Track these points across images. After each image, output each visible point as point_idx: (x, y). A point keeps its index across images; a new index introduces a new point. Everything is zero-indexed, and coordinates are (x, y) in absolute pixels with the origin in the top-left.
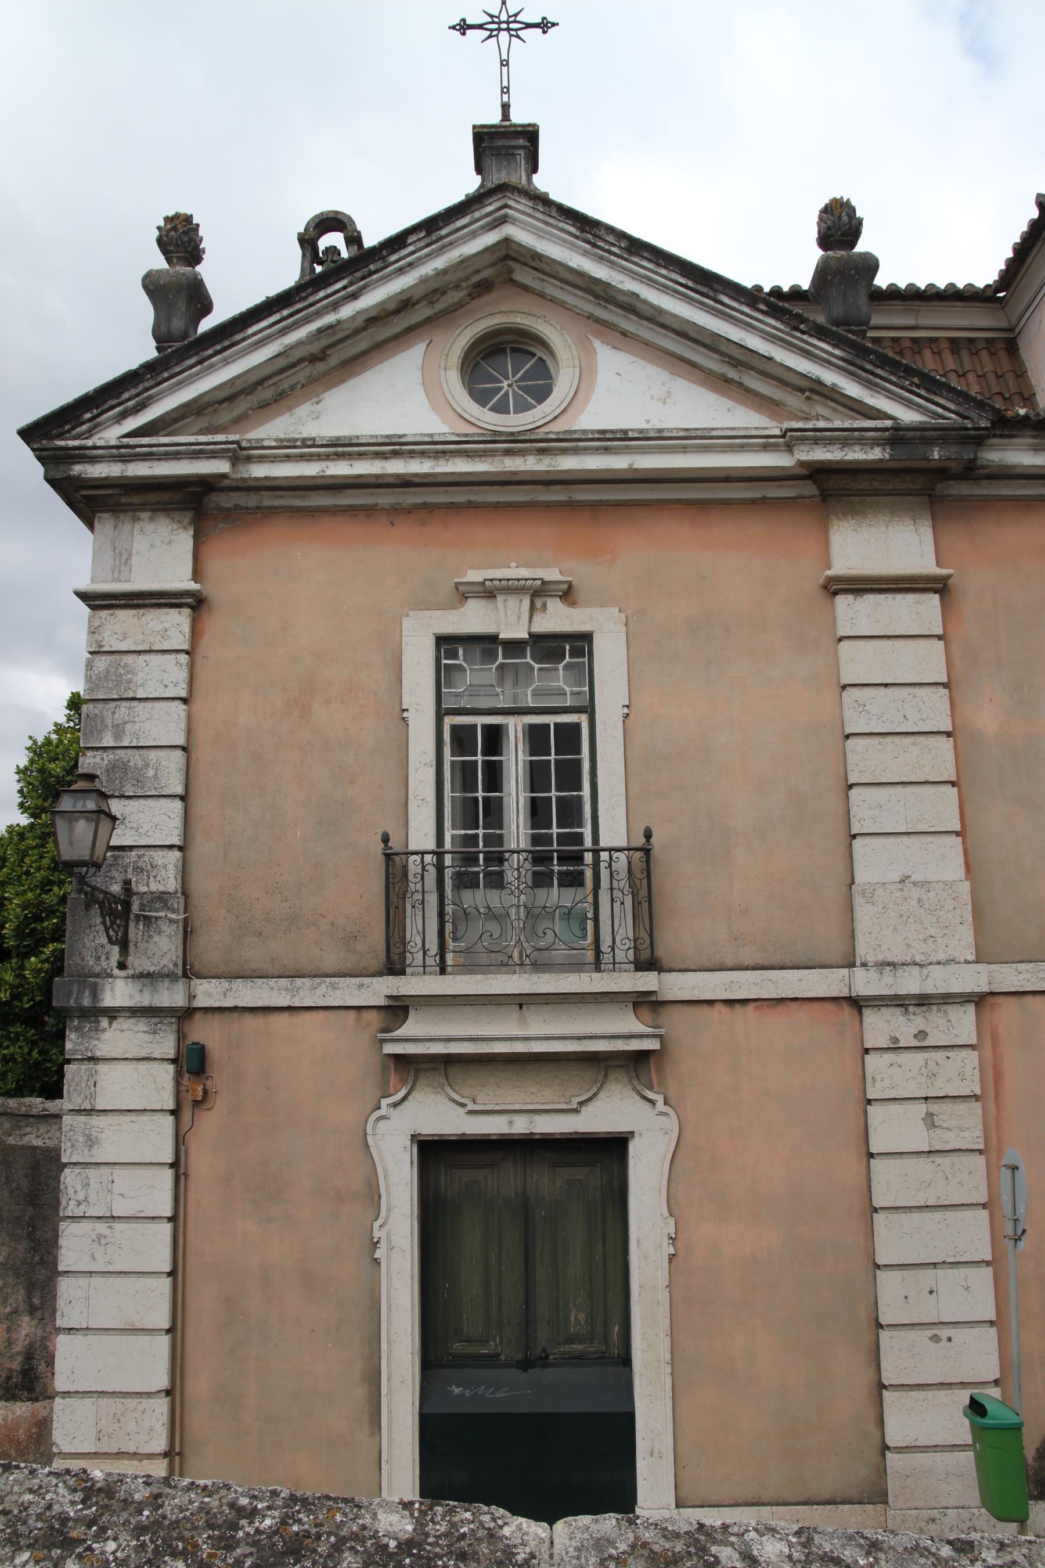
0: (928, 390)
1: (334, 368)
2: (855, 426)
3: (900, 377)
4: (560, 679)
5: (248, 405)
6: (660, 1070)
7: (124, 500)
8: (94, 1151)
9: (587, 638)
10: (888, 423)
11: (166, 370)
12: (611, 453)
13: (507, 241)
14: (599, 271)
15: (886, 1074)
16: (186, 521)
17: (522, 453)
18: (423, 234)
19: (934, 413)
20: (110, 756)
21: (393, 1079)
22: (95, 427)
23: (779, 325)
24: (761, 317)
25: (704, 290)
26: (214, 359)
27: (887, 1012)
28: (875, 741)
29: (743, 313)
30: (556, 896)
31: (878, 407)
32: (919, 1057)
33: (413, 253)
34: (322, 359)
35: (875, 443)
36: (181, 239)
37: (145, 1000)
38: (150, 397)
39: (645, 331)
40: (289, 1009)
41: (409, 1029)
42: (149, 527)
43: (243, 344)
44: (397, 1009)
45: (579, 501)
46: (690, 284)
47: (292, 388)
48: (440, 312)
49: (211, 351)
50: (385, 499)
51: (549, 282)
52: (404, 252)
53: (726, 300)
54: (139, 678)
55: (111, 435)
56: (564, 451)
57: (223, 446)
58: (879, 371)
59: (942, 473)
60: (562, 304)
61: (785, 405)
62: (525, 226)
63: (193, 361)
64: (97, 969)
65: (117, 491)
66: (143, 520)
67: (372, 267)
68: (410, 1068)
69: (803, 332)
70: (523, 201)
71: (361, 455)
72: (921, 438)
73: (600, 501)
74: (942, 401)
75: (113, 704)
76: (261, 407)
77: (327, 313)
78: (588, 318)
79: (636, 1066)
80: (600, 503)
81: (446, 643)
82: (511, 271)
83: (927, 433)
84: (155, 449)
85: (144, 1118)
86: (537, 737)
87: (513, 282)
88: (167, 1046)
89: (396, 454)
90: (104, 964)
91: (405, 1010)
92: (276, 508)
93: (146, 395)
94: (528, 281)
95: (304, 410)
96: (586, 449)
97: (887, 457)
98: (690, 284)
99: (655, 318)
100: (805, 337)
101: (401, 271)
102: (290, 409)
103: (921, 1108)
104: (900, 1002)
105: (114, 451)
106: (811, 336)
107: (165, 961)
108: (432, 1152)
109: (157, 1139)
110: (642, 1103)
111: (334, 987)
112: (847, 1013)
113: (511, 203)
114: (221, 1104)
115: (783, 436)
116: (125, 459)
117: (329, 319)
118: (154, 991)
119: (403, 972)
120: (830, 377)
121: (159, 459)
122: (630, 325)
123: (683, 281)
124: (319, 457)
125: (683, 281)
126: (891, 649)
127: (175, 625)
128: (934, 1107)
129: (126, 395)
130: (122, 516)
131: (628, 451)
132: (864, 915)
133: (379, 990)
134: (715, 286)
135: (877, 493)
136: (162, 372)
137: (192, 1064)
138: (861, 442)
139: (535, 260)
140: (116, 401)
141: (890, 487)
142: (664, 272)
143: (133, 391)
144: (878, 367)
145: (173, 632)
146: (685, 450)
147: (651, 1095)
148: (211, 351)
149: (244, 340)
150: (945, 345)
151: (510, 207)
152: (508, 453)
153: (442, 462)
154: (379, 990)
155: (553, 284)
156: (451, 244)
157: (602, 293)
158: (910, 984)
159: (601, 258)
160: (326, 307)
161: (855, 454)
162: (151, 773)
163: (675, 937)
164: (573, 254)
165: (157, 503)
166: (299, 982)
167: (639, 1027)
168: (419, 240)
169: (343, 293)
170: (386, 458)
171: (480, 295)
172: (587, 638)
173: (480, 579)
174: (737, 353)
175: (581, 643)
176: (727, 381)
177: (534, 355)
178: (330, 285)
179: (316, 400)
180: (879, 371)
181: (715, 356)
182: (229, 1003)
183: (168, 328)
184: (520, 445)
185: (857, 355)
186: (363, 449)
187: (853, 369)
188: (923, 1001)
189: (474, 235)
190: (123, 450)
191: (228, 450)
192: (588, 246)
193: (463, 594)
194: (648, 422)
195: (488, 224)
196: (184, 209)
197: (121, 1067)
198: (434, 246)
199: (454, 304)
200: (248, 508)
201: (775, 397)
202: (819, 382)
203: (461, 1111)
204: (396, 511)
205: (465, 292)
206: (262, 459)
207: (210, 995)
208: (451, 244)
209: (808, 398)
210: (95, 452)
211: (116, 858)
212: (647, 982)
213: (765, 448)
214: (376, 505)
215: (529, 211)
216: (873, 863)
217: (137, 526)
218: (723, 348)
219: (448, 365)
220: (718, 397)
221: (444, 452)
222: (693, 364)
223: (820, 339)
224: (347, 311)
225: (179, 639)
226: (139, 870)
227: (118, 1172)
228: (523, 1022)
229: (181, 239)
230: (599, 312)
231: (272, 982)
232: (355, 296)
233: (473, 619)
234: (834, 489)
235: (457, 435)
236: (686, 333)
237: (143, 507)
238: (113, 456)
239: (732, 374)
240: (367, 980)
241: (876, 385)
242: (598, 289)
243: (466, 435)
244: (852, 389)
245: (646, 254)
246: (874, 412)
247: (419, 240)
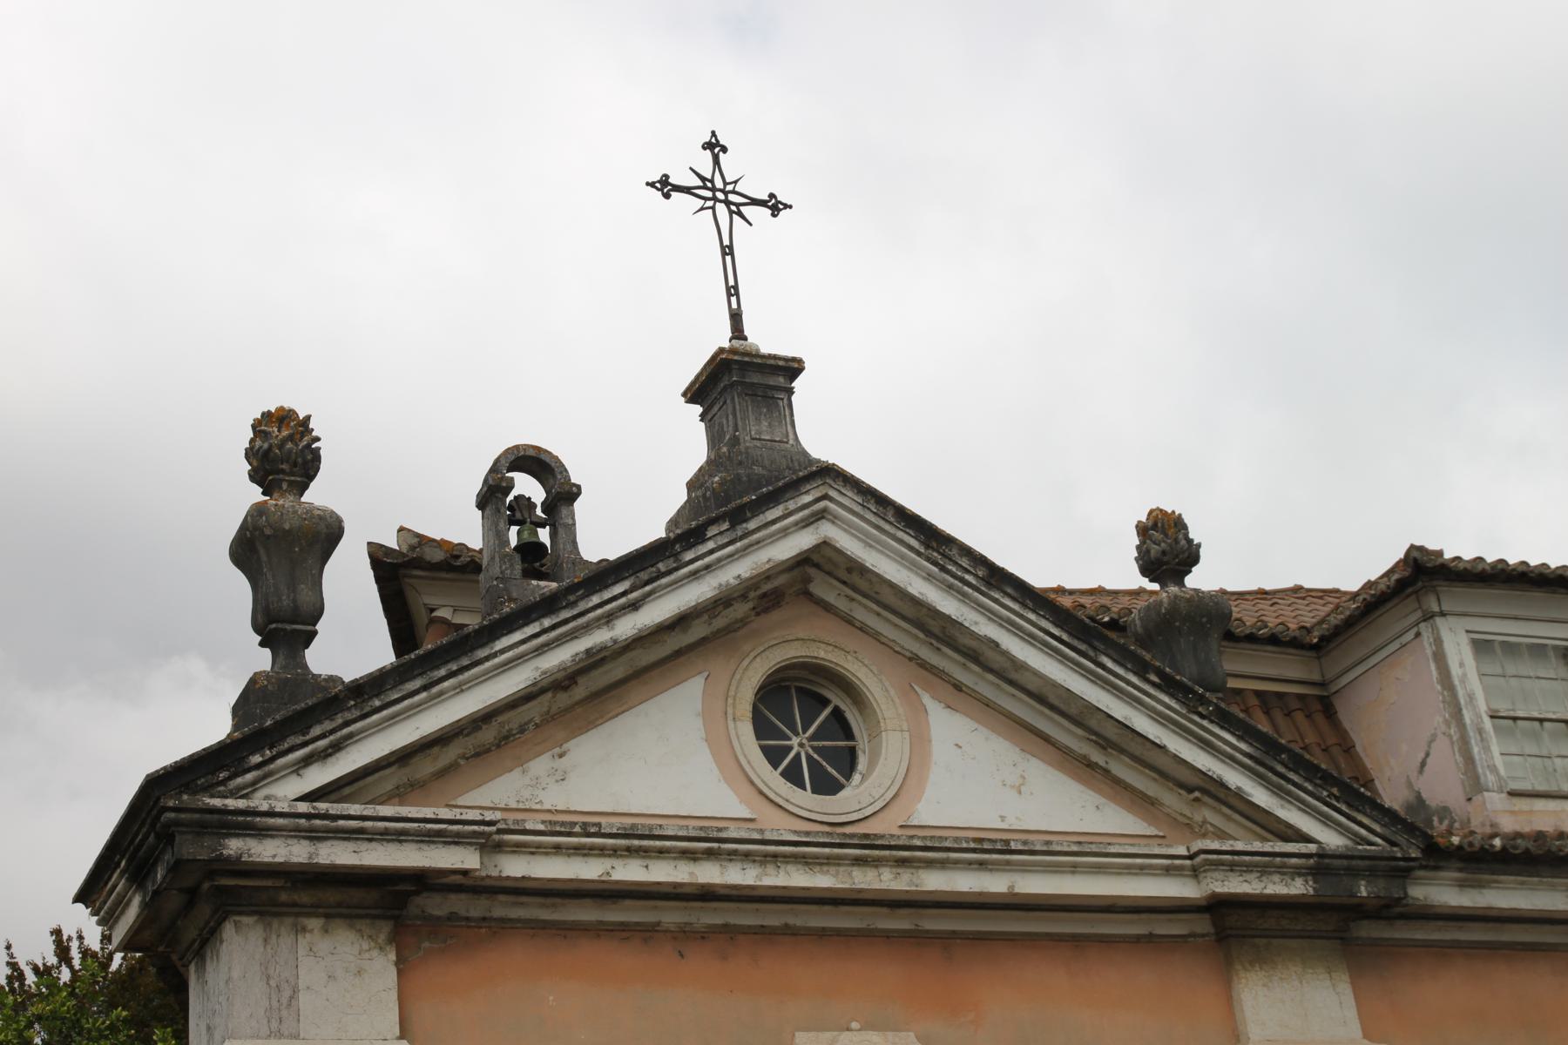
0: (1349, 805)
1: (578, 703)
2: (1277, 849)
3: (1316, 785)
5: (461, 751)
7: (284, 897)
10: (1312, 848)
11: (377, 696)
12: (987, 870)
13: (825, 544)
14: (948, 605)
16: (382, 938)
17: (876, 863)
18: (726, 526)
19: (1356, 834)
22: (265, 777)
23: (1173, 703)
24: (1152, 691)
25: (1083, 647)
26: (446, 684)
29: (1128, 683)
31: (1292, 822)
33: (711, 552)
34: (566, 688)
35: (1298, 872)
38: (351, 736)
39: (986, 686)
42: (324, 945)
43: (488, 665)
45: (928, 931)
46: (1065, 637)
47: (522, 730)
48: (719, 631)
49: (443, 672)
50: (671, 916)
51: (860, 603)
52: (702, 549)
53: (1110, 664)
56: (930, 864)
57: (476, 828)
58: (1292, 776)
59: (1360, 911)
60: (875, 636)
61: (1162, 804)
62: (849, 528)
63: (417, 683)
65: (280, 883)
66: (311, 931)
67: (662, 566)
69: (1202, 717)
70: (849, 494)
72: (1348, 869)
73: (954, 932)
74: (1366, 821)
76: (477, 755)
77: (599, 627)
78: (910, 659)
80: (954, 935)
82: (808, 580)
83: (1354, 863)
84: (368, 824)
87: (808, 595)
89: (710, 854)
92: (511, 920)
93: (346, 731)
94: (831, 598)
95: (541, 765)
96: (957, 862)
97: (1311, 892)
98: (1065, 637)
99: (1009, 673)
100: (1205, 723)
101: (695, 575)
102: (521, 762)
105: (303, 821)
106: (1212, 722)
113: (833, 493)
115: (1190, 857)
116: (314, 836)
117: (600, 637)
120: (1234, 778)
121: (370, 840)
122: (968, 676)
123: (1056, 631)
124: (602, 852)
125: (1056, 631)
129: (316, 731)
130: (275, 923)
131: (1007, 867)
134: (1096, 644)
136: (370, 698)
138: (1282, 870)
139: (853, 574)
140: (300, 739)
141: (1299, 927)
142: (1032, 616)
143: (328, 725)
144: (1290, 770)
146: (1074, 869)
148: (443, 672)
149: (487, 659)
151: (831, 499)
152: (859, 862)
153: (770, 869)
155: (865, 607)
156: (758, 542)
157: (936, 630)
159: (950, 587)
160: (598, 619)
161: (1276, 887)
164: (912, 575)
165: (339, 905)
168: (721, 533)
169: (623, 600)
170: (695, 860)
171: (766, 610)
174: (1111, 732)
176: (1091, 765)
178: (607, 587)
179: (557, 750)
180: (1292, 776)
181: (1080, 732)
183: (294, 601)
184: (877, 852)
185: (1267, 753)
186: (668, 843)
187: (1261, 770)
189: (785, 533)
190: (318, 822)
191: (482, 834)
192: (935, 569)
194: (1003, 818)
195: (802, 520)
198: (738, 544)
199: (736, 621)
200: (467, 919)
201: (1150, 793)
202: (1221, 784)
204: (686, 936)
205: (750, 605)
206: (519, 848)
208: (758, 542)
209: (1196, 800)
210: (271, 821)
213: (1168, 871)
214: (658, 924)
215: (858, 509)
217: (303, 941)
218: (1093, 723)
219: (738, 714)
220: (1082, 788)
221: (775, 856)
222: (1046, 739)
223: (1222, 728)
224: (626, 627)
229: (283, 451)
230: (926, 654)
232: (635, 606)
234: (1233, 931)
235: (795, 832)
236: (1046, 697)
237: (313, 910)
238: (298, 829)
239: (1097, 757)
241: (1289, 793)
242: (934, 626)
243: (807, 833)
244: (1261, 797)
245: (1009, 590)
246: (1282, 827)
247: (721, 533)
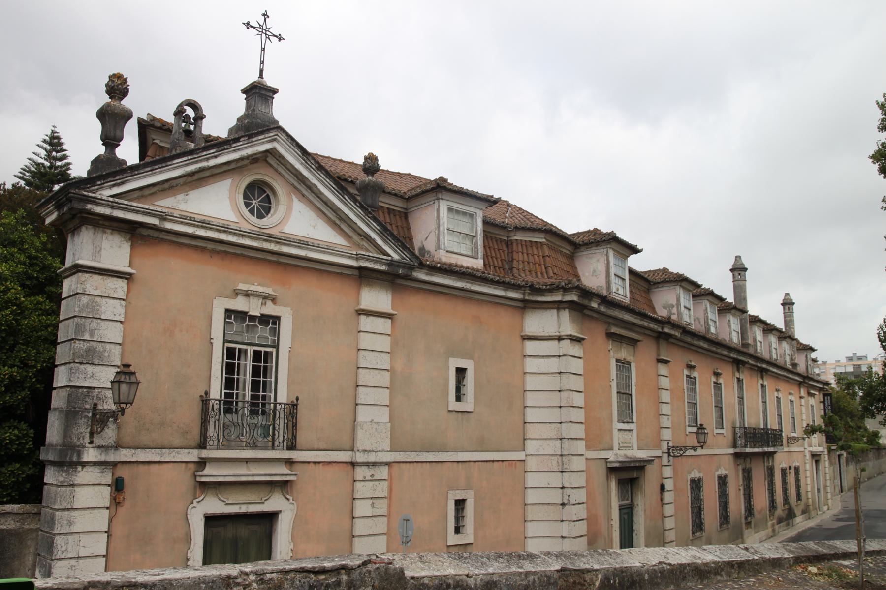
4: (263, 332)
6: (291, 487)
8: (72, 527)
9: (279, 318)
13: (274, 149)
14: (305, 173)
15: (362, 489)
17: (270, 242)
20: (87, 345)
21: (198, 492)
27: (363, 468)
28: (368, 370)
30: (260, 420)
32: (371, 483)
35: (384, 264)
36: (117, 87)
37: (103, 458)
39: (311, 197)
40: (160, 462)
41: (207, 471)
42: (111, 237)
44: (202, 463)
47: (177, 186)
50: (210, 246)
54: (103, 309)
55: (106, 193)
56: (285, 244)
60: (283, 176)
62: (282, 145)
64: (78, 444)
68: (205, 487)
71: (211, 229)
75: (90, 320)
79: (283, 486)
80: (288, 264)
81: (229, 312)
85: (96, 511)
86: (257, 355)
88: (108, 479)
89: (225, 231)
90: (81, 441)
91: (205, 463)
94: (272, 163)
95: (180, 197)
99: (319, 195)
101: (235, 151)
102: (175, 195)
103: (370, 501)
104: (367, 464)
107: (110, 441)
108: (210, 520)
109: (101, 520)
110: (285, 500)
111: (178, 453)
112: (350, 467)
114: (127, 504)
116: (113, 208)
118: (107, 454)
119: (205, 448)
120: (374, 235)
124: (194, 226)
126: (375, 336)
127: (119, 287)
128: (374, 501)
129: (118, 177)
132: (360, 434)
133: (193, 455)
135: (377, 279)
137: (118, 486)
139: (280, 158)
143: (121, 177)
145: (119, 290)
146: (324, 252)
147: (288, 497)
150: (386, 210)
154: (193, 455)
158: (372, 458)
161: (378, 267)
162: (107, 354)
163: (302, 438)
166: (164, 450)
167: (287, 471)
172: (279, 318)
173: (246, 289)
175: (276, 319)
176: (335, 224)
177: (265, 192)
182: (134, 459)
188: (375, 464)
189: (263, 143)
193: (237, 293)
196: (115, 71)
197: (86, 488)
202: (370, 237)
203: (223, 504)
204: (214, 252)
206: (171, 221)
207: (126, 456)
211: (88, 392)
212: (287, 454)
213: (350, 257)
216: (363, 414)
217: (105, 236)
222: (325, 214)
224: (212, 163)
225: (121, 294)
226: (99, 399)
227: (82, 536)
228: (248, 468)
230: (296, 184)
231: (153, 451)
232: (216, 157)
233: (240, 304)
234: (364, 276)
239: (338, 222)
240: (191, 451)
242: (300, 177)
244: (379, 242)
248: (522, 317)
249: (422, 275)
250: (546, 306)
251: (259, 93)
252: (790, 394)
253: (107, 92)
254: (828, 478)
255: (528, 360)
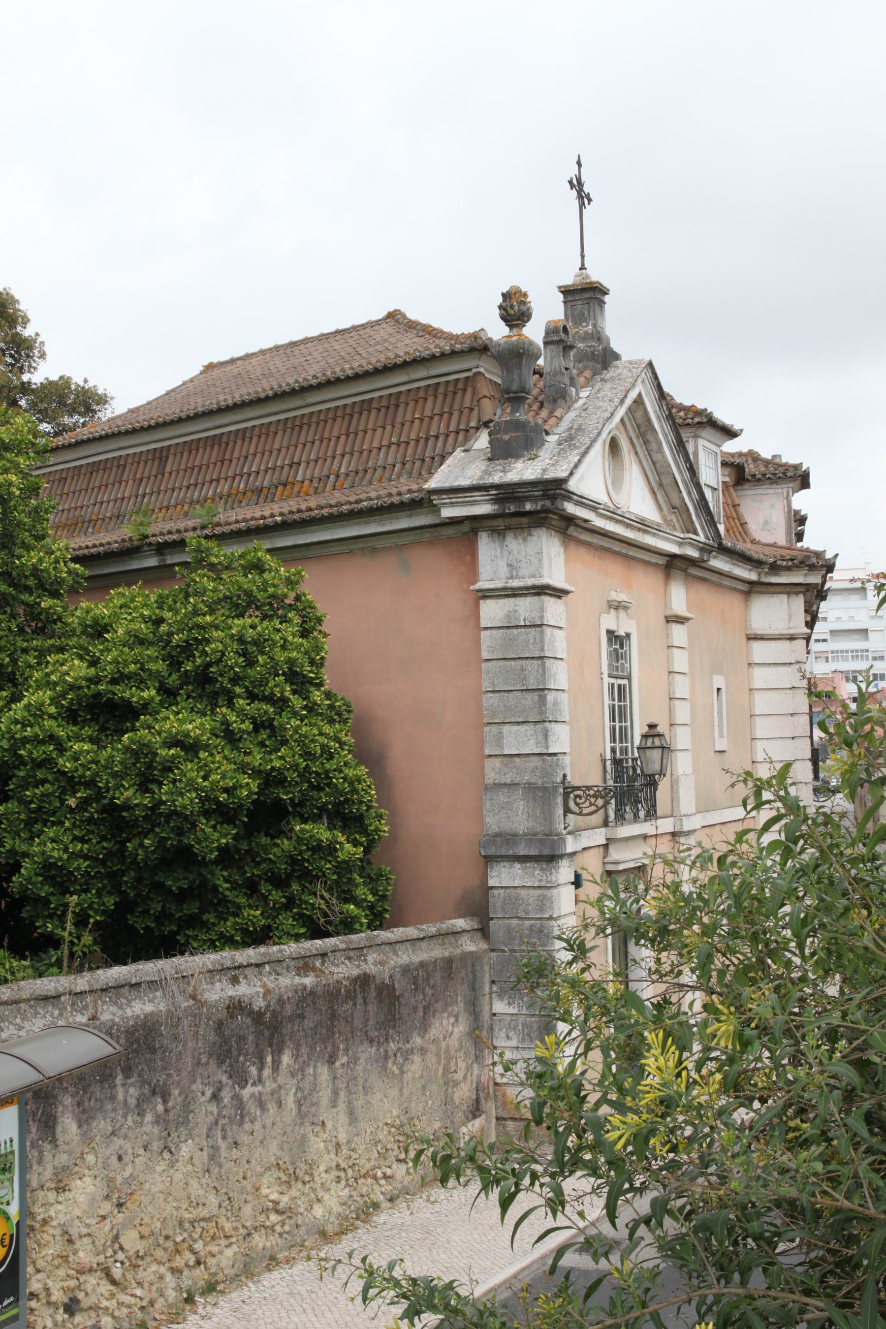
17: (645, 531)
135: (766, 593)
248: (746, 606)
249: (719, 563)
250: (773, 589)
251: (585, 296)
252: (617, 606)
253: (503, 318)
254: (167, 537)
255: (756, 670)
